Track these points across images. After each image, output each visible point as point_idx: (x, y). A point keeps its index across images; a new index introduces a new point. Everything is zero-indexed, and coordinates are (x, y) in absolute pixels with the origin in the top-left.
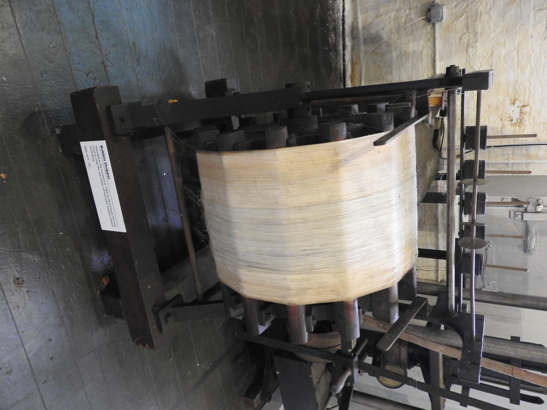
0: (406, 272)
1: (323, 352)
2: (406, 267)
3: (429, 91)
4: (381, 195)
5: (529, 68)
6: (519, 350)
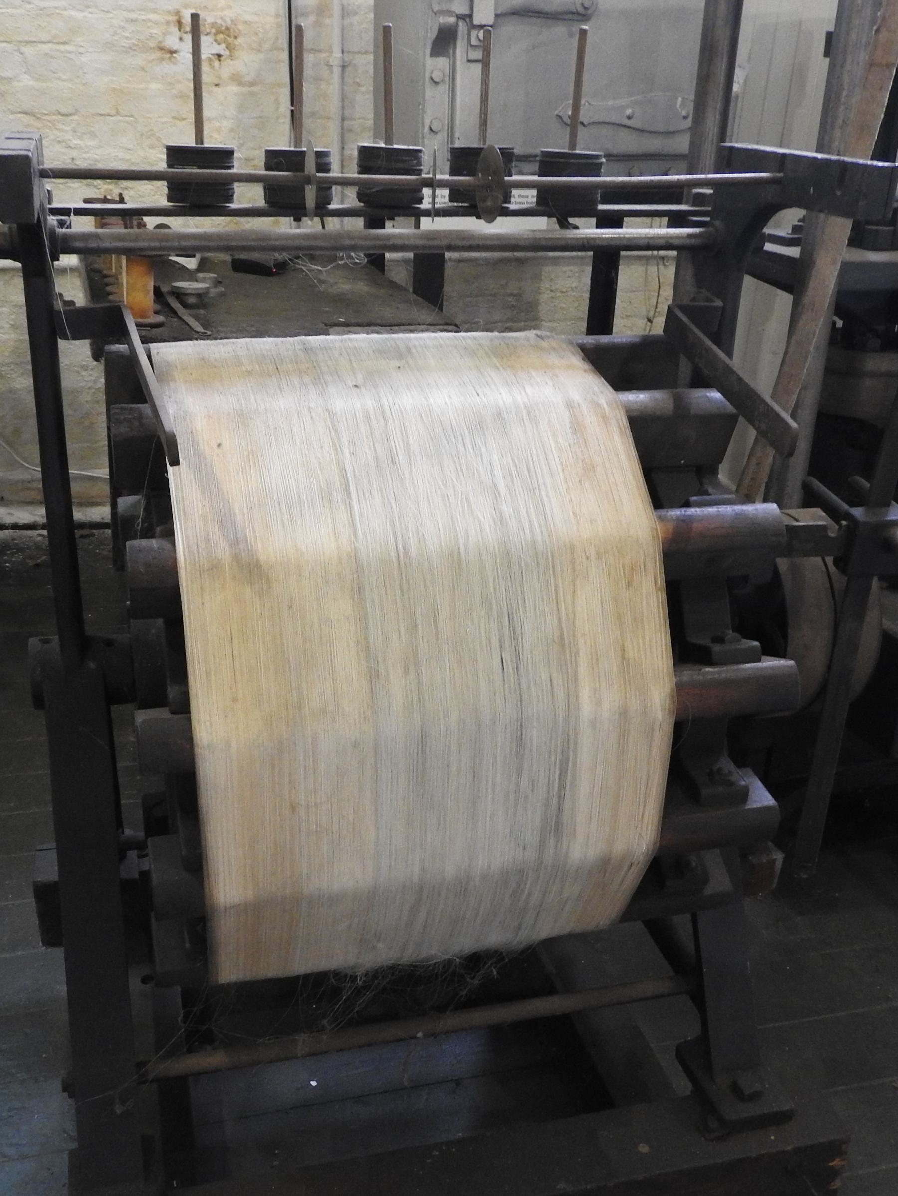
0: (586, 366)
1: (847, 606)
2: (570, 367)
3: (59, 306)
4: (345, 440)
5: (73, 13)
6: (853, 36)
